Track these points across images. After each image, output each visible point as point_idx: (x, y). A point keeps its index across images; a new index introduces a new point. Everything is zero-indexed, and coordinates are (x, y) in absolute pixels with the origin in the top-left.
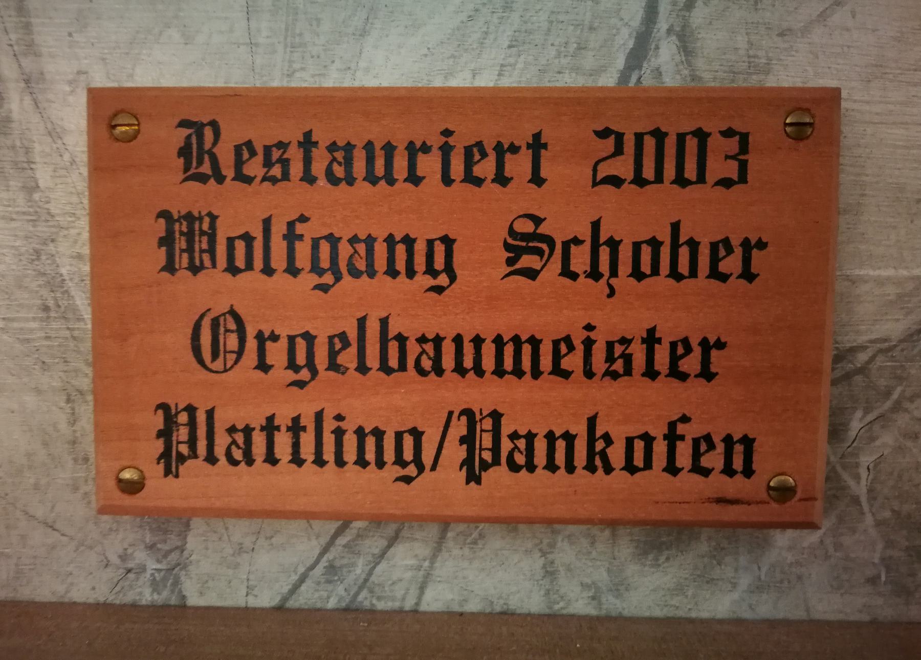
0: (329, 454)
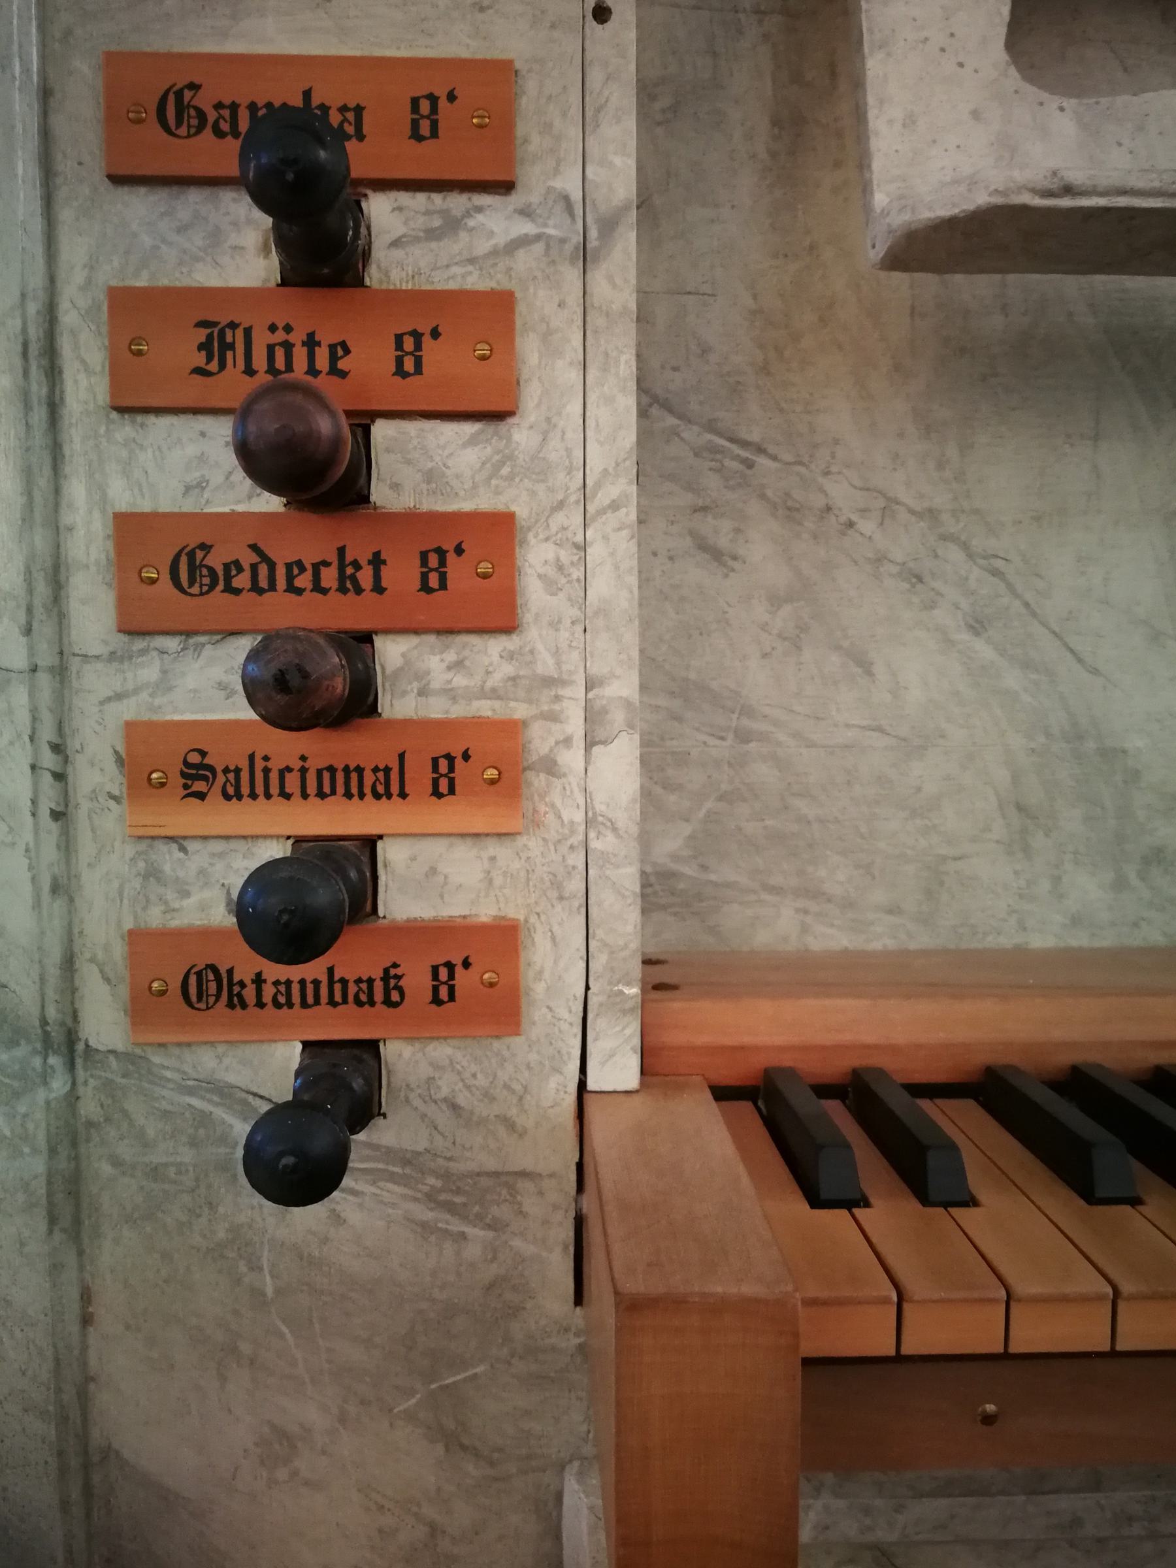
0: (260, 789)
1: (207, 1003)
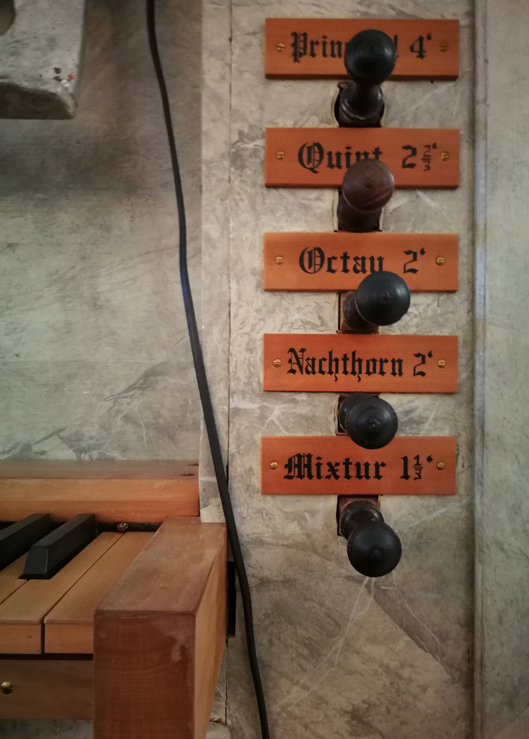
1: (314, 164)
